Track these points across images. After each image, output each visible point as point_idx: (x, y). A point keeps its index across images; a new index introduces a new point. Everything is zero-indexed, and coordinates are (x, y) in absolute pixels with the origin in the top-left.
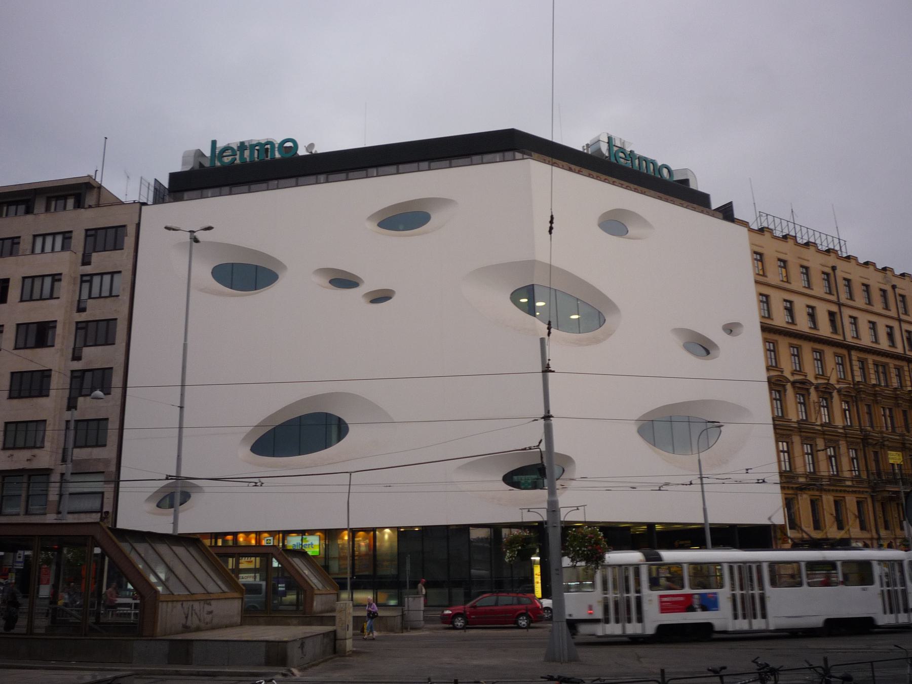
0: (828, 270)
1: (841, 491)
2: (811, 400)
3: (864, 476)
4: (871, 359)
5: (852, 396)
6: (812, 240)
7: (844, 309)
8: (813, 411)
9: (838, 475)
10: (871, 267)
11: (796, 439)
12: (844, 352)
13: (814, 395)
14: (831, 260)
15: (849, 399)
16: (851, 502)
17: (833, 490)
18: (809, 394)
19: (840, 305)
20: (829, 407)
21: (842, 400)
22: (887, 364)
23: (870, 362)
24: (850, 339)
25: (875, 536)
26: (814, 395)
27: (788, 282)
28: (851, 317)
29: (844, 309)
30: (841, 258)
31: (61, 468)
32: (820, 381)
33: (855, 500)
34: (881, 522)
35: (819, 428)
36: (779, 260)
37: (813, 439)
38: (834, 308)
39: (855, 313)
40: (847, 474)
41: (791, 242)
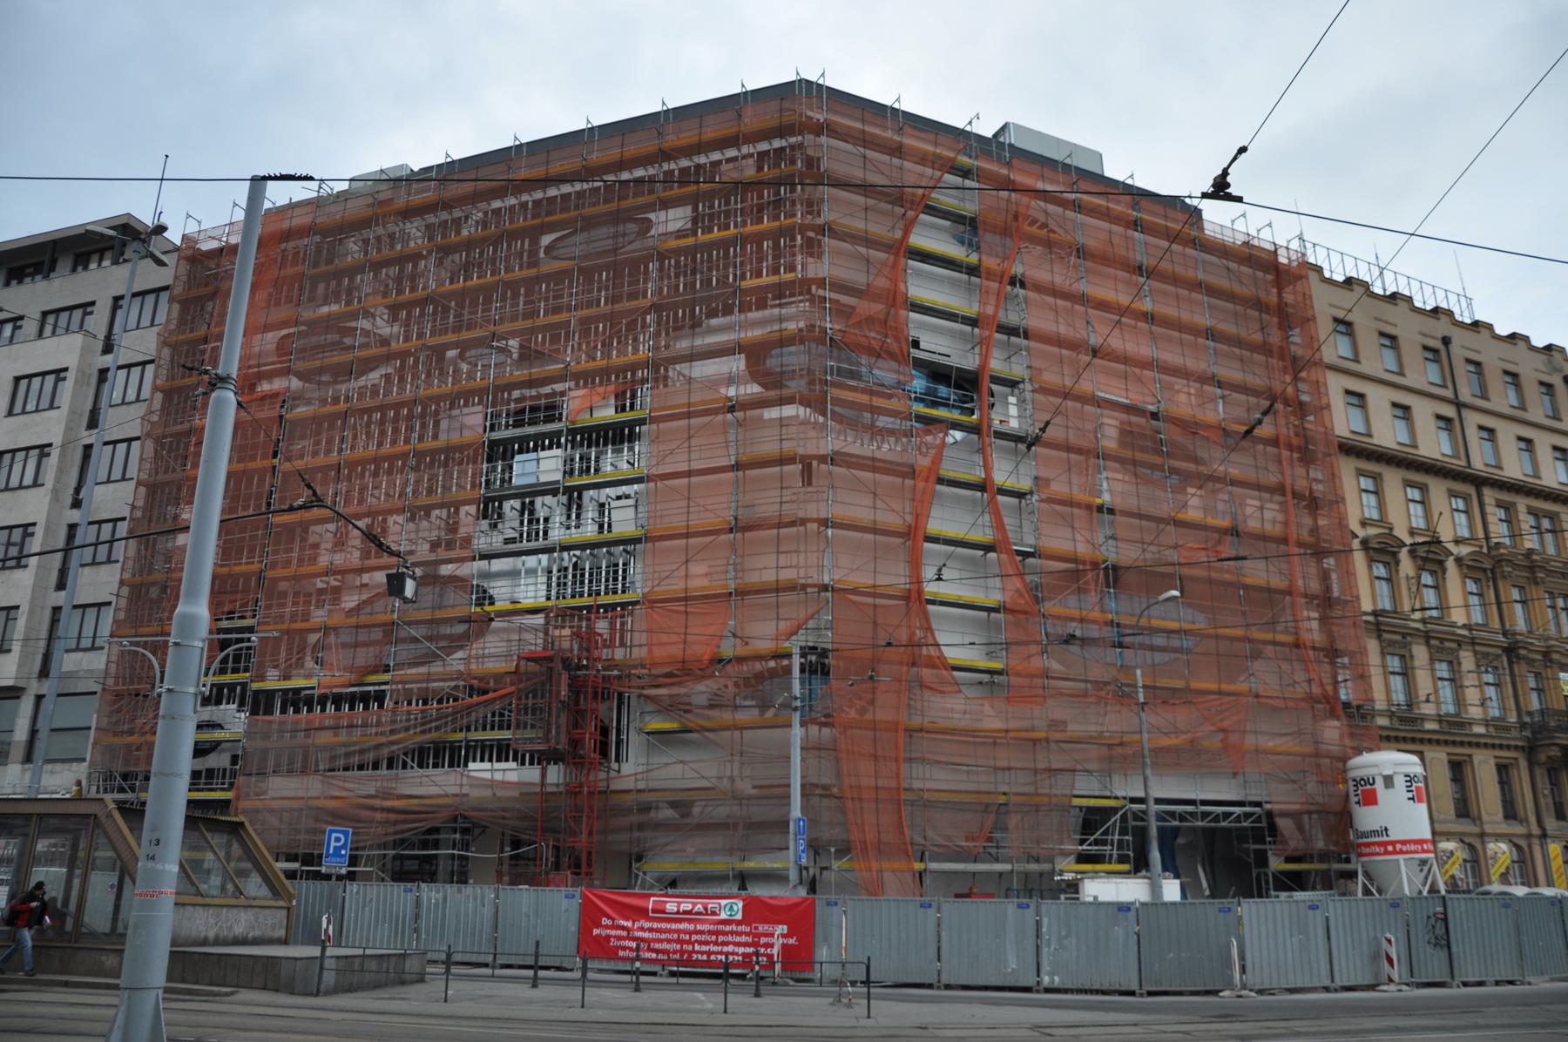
0: (1438, 344)
1: (1462, 744)
2: (1402, 574)
3: (1513, 718)
4: (1522, 503)
5: (1484, 570)
6: (1444, 305)
7: (1466, 413)
8: (1405, 592)
9: (1458, 715)
10: (1521, 344)
11: (1420, 653)
12: (1470, 490)
13: (1406, 566)
14: (1441, 328)
15: (1479, 575)
16: (1484, 767)
17: (1446, 743)
18: (1397, 563)
19: (1460, 406)
20: (1438, 588)
21: (1371, 561)
22: (1514, 504)
23: (1522, 508)
24: (1478, 464)
25: (1536, 831)
26: (1406, 566)
27: (1401, 374)
28: (1481, 428)
29: (1466, 413)
30: (1461, 325)
31: (35, 687)
32: (1372, 531)
33: (1492, 762)
34: (1546, 802)
35: (1419, 626)
36: (1506, 372)
37: (1406, 645)
38: (1449, 411)
39: (1489, 422)
40: (1475, 712)
41: (1359, 291)
